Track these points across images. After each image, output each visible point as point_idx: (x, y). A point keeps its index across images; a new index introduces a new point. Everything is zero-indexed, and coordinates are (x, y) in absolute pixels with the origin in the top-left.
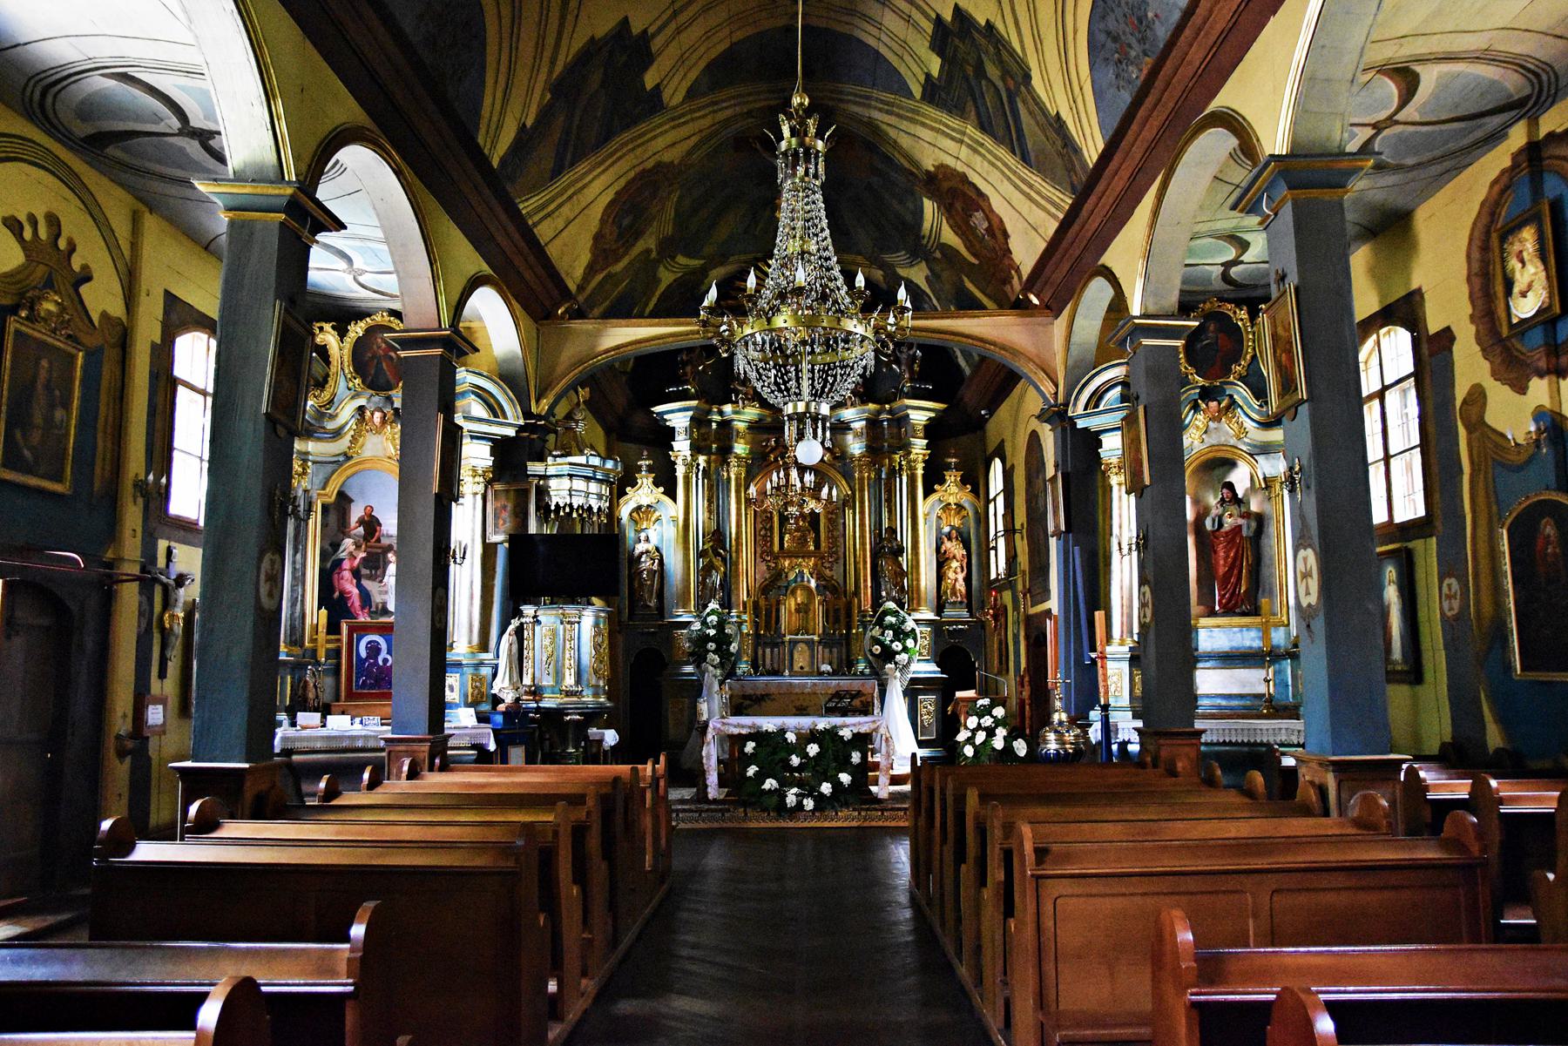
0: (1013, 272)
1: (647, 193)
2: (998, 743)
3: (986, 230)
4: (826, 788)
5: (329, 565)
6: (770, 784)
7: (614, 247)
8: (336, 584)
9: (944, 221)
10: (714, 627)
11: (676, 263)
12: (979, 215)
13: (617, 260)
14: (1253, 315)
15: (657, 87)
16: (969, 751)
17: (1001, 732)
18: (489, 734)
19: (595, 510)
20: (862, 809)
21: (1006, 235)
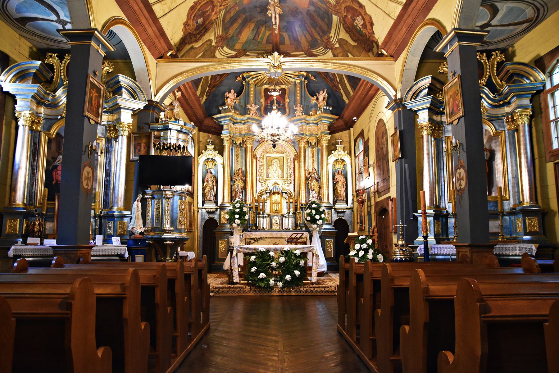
0: (374, 44)
1: (209, 8)
2: (370, 256)
3: (362, 25)
4: (288, 277)
5: (51, 168)
6: (262, 275)
7: (195, 33)
8: (54, 176)
9: (342, 25)
10: (238, 208)
11: (224, 51)
12: (359, 18)
13: (197, 41)
14: (489, 57)
16: (357, 260)
17: (371, 251)
18: (126, 249)
19: (182, 147)
20: (305, 287)
21: (372, 24)
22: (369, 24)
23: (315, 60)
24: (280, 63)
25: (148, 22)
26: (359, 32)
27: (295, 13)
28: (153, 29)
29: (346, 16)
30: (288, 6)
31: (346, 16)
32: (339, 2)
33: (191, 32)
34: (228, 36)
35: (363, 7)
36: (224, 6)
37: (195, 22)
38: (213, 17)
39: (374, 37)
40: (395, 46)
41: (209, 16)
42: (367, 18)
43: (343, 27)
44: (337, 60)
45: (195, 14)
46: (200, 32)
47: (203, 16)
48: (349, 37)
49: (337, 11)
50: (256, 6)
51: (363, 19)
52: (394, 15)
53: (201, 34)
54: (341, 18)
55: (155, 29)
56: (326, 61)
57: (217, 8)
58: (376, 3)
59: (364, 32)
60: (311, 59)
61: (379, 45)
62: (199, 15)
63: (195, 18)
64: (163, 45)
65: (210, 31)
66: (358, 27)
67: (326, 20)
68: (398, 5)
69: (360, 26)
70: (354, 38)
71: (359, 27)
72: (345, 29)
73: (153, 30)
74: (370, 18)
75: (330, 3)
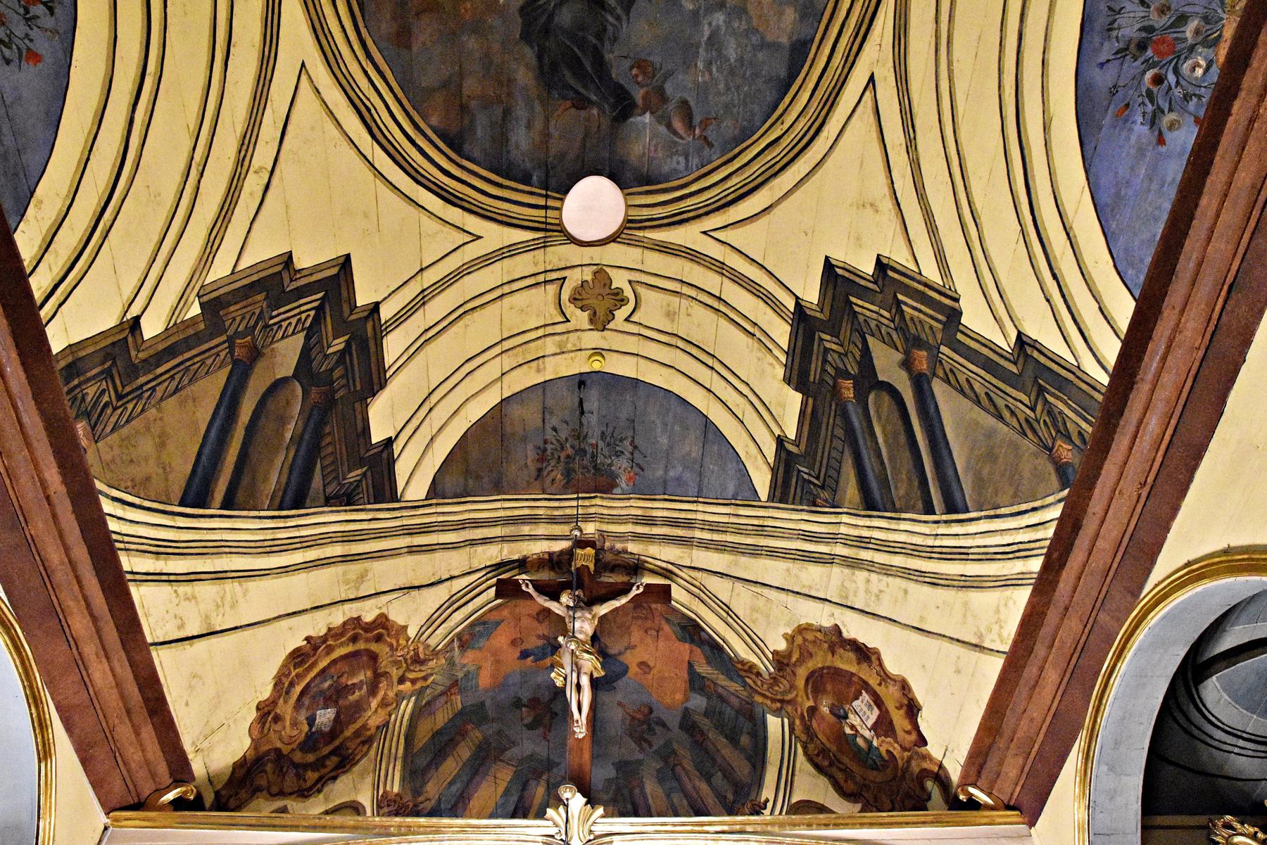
0: (929, 784)
1: (361, 677)
3: (875, 727)
7: (298, 757)
9: (800, 750)
15: (389, 442)
21: (912, 709)
22: (902, 712)
23: (726, 828)
24: (592, 837)
25: (98, 631)
26: (866, 756)
27: (645, 727)
28: (118, 670)
29: (813, 710)
30: (620, 704)
31: (813, 710)
32: (785, 661)
33: (286, 750)
34: (422, 806)
35: (874, 658)
36: (413, 682)
37: (302, 717)
38: (373, 717)
39: (927, 757)
40: (1020, 761)
41: (359, 707)
42: (890, 695)
43: (806, 753)
44: (809, 825)
45: (308, 685)
46: (318, 765)
47: (336, 702)
48: (831, 789)
49: (779, 697)
50: (519, 700)
51: (878, 701)
52: (1000, 635)
53: (323, 771)
54: (798, 722)
55: (126, 673)
56: (769, 828)
57: (390, 685)
58: (922, 619)
59: (883, 750)
60: (710, 824)
61: (948, 778)
62: (322, 692)
63: (306, 701)
64: (150, 756)
65: (356, 769)
66: (860, 741)
67: (745, 740)
68: (1009, 592)
69: (867, 734)
70: (850, 786)
71: (865, 739)
72: (810, 759)
73: (114, 676)
74: (904, 686)
75: (759, 674)
